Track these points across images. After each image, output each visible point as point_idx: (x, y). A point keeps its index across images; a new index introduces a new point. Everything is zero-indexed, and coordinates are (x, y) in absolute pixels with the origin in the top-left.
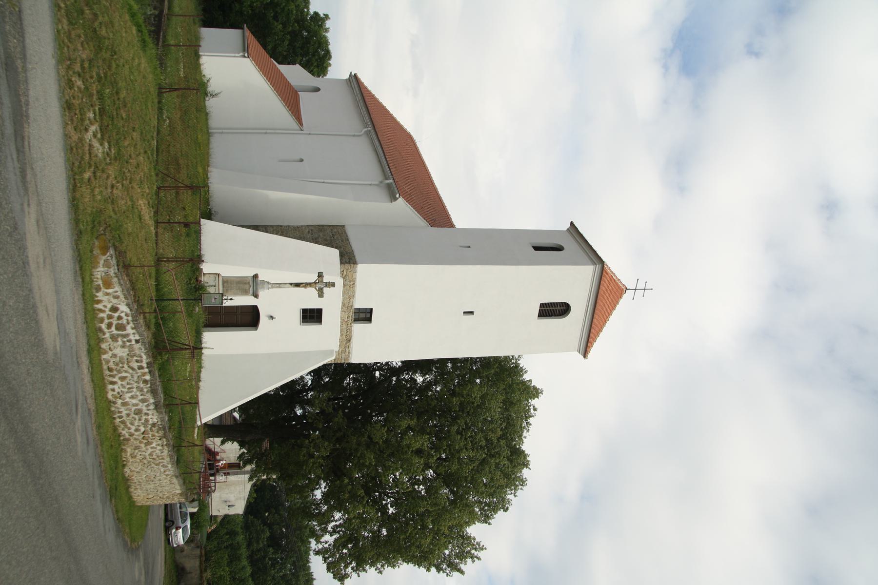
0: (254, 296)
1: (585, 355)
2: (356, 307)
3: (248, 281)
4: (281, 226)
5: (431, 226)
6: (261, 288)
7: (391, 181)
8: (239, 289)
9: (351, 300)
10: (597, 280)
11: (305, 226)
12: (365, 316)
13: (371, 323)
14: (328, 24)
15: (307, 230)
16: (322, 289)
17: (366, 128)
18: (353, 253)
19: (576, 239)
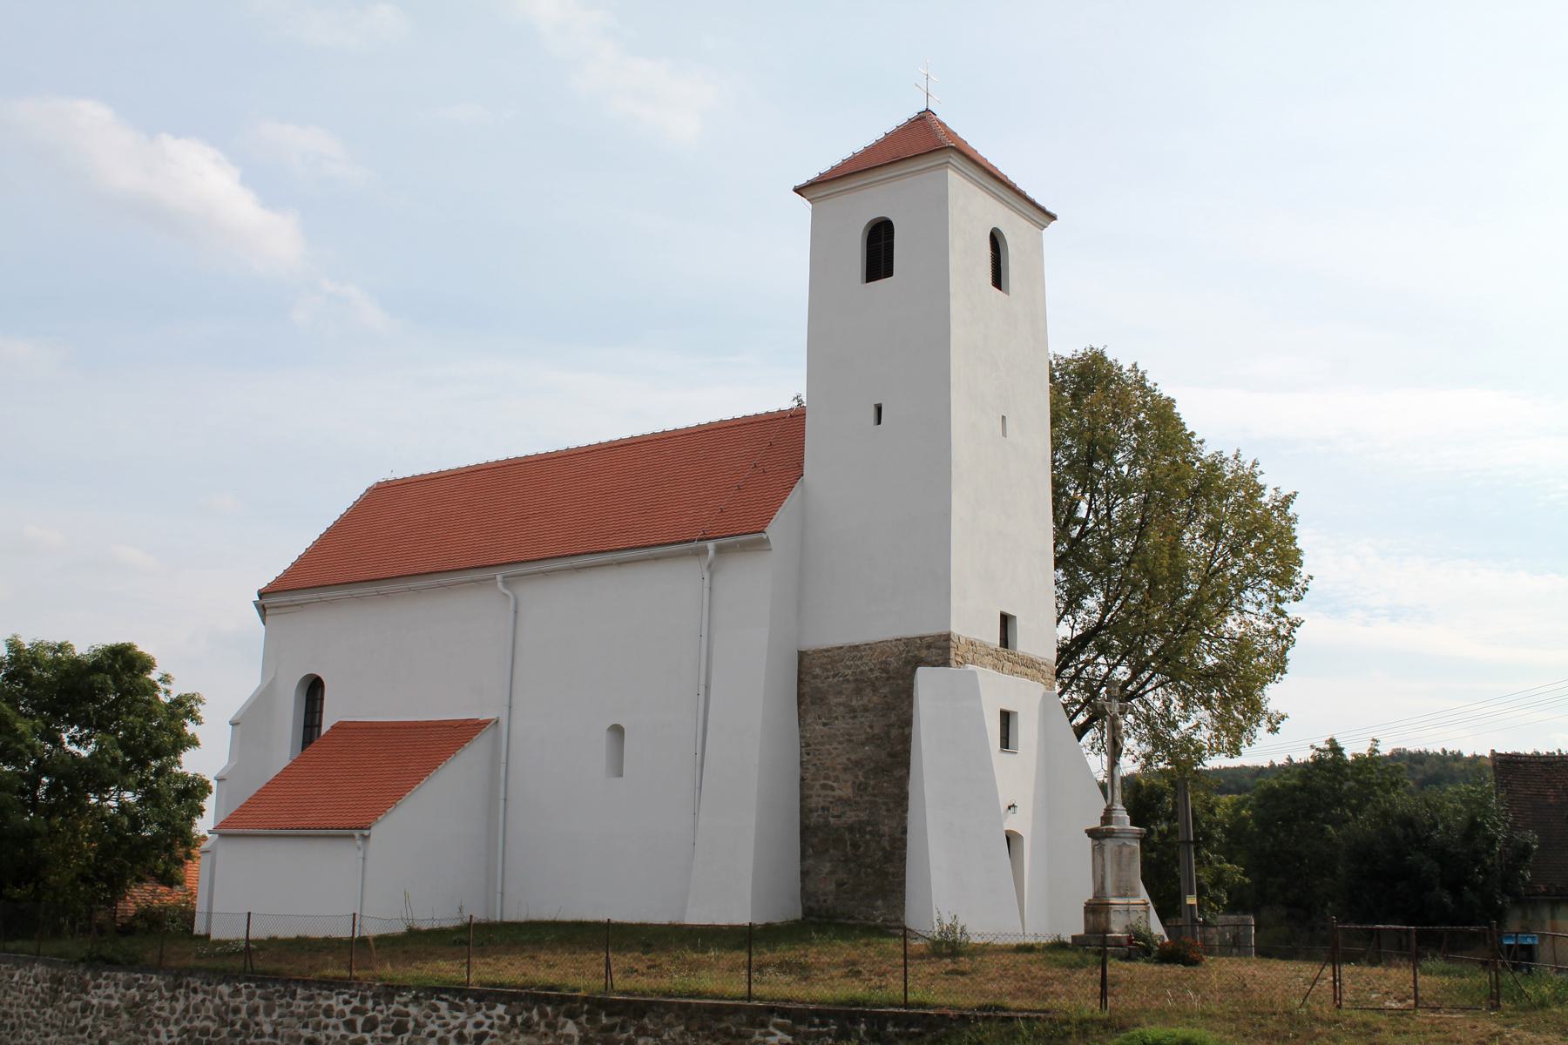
1: (1053, 217)
2: (998, 642)
3: (1117, 848)
4: (802, 779)
5: (802, 475)
7: (711, 545)
8: (1129, 866)
13: (1015, 617)
14: (26, 642)
18: (909, 639)
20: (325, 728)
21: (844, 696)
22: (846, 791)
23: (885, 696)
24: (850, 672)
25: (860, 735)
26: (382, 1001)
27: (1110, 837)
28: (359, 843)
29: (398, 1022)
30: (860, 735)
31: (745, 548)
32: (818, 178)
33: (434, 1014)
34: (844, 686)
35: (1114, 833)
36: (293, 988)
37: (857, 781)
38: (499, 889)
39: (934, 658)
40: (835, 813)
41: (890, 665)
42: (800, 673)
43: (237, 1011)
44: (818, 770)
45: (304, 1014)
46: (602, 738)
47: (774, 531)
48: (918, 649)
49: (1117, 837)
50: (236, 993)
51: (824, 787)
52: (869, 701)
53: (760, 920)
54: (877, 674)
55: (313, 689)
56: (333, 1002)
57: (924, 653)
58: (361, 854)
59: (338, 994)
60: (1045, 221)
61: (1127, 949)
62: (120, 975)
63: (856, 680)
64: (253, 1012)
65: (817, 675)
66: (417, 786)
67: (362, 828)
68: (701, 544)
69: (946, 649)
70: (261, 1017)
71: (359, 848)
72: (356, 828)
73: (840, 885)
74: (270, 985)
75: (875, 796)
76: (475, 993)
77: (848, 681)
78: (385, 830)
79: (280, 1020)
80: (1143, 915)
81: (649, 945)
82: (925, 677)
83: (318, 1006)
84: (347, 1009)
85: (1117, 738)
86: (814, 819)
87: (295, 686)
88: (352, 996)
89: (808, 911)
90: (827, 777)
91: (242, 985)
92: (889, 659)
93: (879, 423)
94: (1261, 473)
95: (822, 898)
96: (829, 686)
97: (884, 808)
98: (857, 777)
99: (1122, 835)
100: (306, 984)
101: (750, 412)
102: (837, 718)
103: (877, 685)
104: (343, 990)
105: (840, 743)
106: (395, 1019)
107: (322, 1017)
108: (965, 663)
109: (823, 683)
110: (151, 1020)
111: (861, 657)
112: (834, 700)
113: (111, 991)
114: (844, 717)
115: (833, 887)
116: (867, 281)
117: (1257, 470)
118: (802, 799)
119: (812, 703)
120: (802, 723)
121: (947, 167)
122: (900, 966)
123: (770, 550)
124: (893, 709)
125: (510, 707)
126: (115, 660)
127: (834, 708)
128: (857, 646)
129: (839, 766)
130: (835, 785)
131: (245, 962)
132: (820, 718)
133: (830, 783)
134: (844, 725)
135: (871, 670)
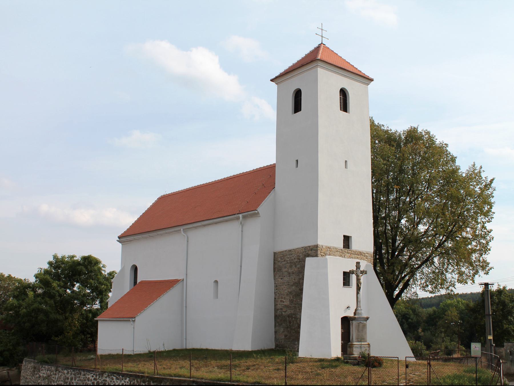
0: (367, 320)
1: (372, 80)
2: (342, 246)
3: (357, 324)
4: (275, 298)
5: (275, 188)
6: (361, 315)
7: (241, 215)
8: (362, 330)
9: (338, 250)
10: (327, 65)
11: (275, 281)
12: (347, 240)
14: (60, 256)
15: (280, 280)
16: (361, 271)
17: (181, 232)
18: (305, 247)
19: (288, 78)
20: (138, 283)
21: (287, 268)
22: (287, 303)
23: (299, 268)
24: (288, 259)
25: (291, 282)
26: (101, 376)
27: (354, 320)
28: (132, 323)
29: (104, 383)
30: (291, 282)
31: (252, 216)
32: (280, 75)
33: (112, 381)
34: (287, 265)
35: (356, 318)
36: (81, 371)
37: (291, 299)
38: (185, 338)
39: (313, 254)
40: (284, 311)
41: (300, 257)
42: (274, 260)
43: (68, 379)
44: (279, 295)
45: (83, 380)
46: (212, 284)
47: (261, 209)
48: (308, 251)
49: (357, 320)
50: (68, 373)
51: (281, 301)
52: (294, 270)
53: (256, 349)
54: (296, 260)
55: (135, 269)
56: (89, 376)
57: (310, 252)
58: (133, 326)
59: (91, 374)
60: (369, 82)
61: (357, 361)
62: (46, 367)
63: (290, 263)
64: (72, 379)
65: (279, 261)
66: (152, 303)
67: (132, 318)
68: (238, 215)
69: (317, 251)
70: (73, 381)
71: (132, 325)
72: (131, 318)
73: (286, 336)
74: (76, 370)
75: (295, 304)
76: (122, 374)
77: (288, 263)
78: (140, 319)
79: (78, 382)
80: (368, 348)
81: (206, 358)
82: (309, 261)
83: (86, 378)
84: (93, 378)
85: (359, 283)
86: (279, 313)
87: (130, 270)
88: (94, 374)
89: (277, 346)
90: (282, 298)
91: (69, 370)
92: (300, 255)
93: (297, 166)
94: (484, 171)
95: (280, 341)
96: (283, 265)
97: (298, 309)
98: (290, 297)
99: (359, 319)
100: (84, 370)
101: (262, 166)
102: (285, 276)
103: (296, 264)
104: (92, 373)
105: (286, 285)
106: (104, 382)
107: (87, 381)
108: (326, 255)
109: (281, 264)
110: (51, 381)
111: (292, 254)
112: (284, 270)
113: (44, 372)
114: (287, 276)
115: (283, 337)
116: (295, 113)
117: (482, 170)
118: (275, 306)
119: (278, 271)
120: (275, 278)
121: (318, 67)
122: (159, 370)
123: (260, 216)
124: (301, 273)
125: (187, 275)
126: (85, 261)
127: (284, 273)
128: (291, 250)
129: (285, 294)
130: (284, 300)
131: (73, 362)
132: (280, 277)
133: (283, 300)
134: (287, 279)
135: (295, 259)
